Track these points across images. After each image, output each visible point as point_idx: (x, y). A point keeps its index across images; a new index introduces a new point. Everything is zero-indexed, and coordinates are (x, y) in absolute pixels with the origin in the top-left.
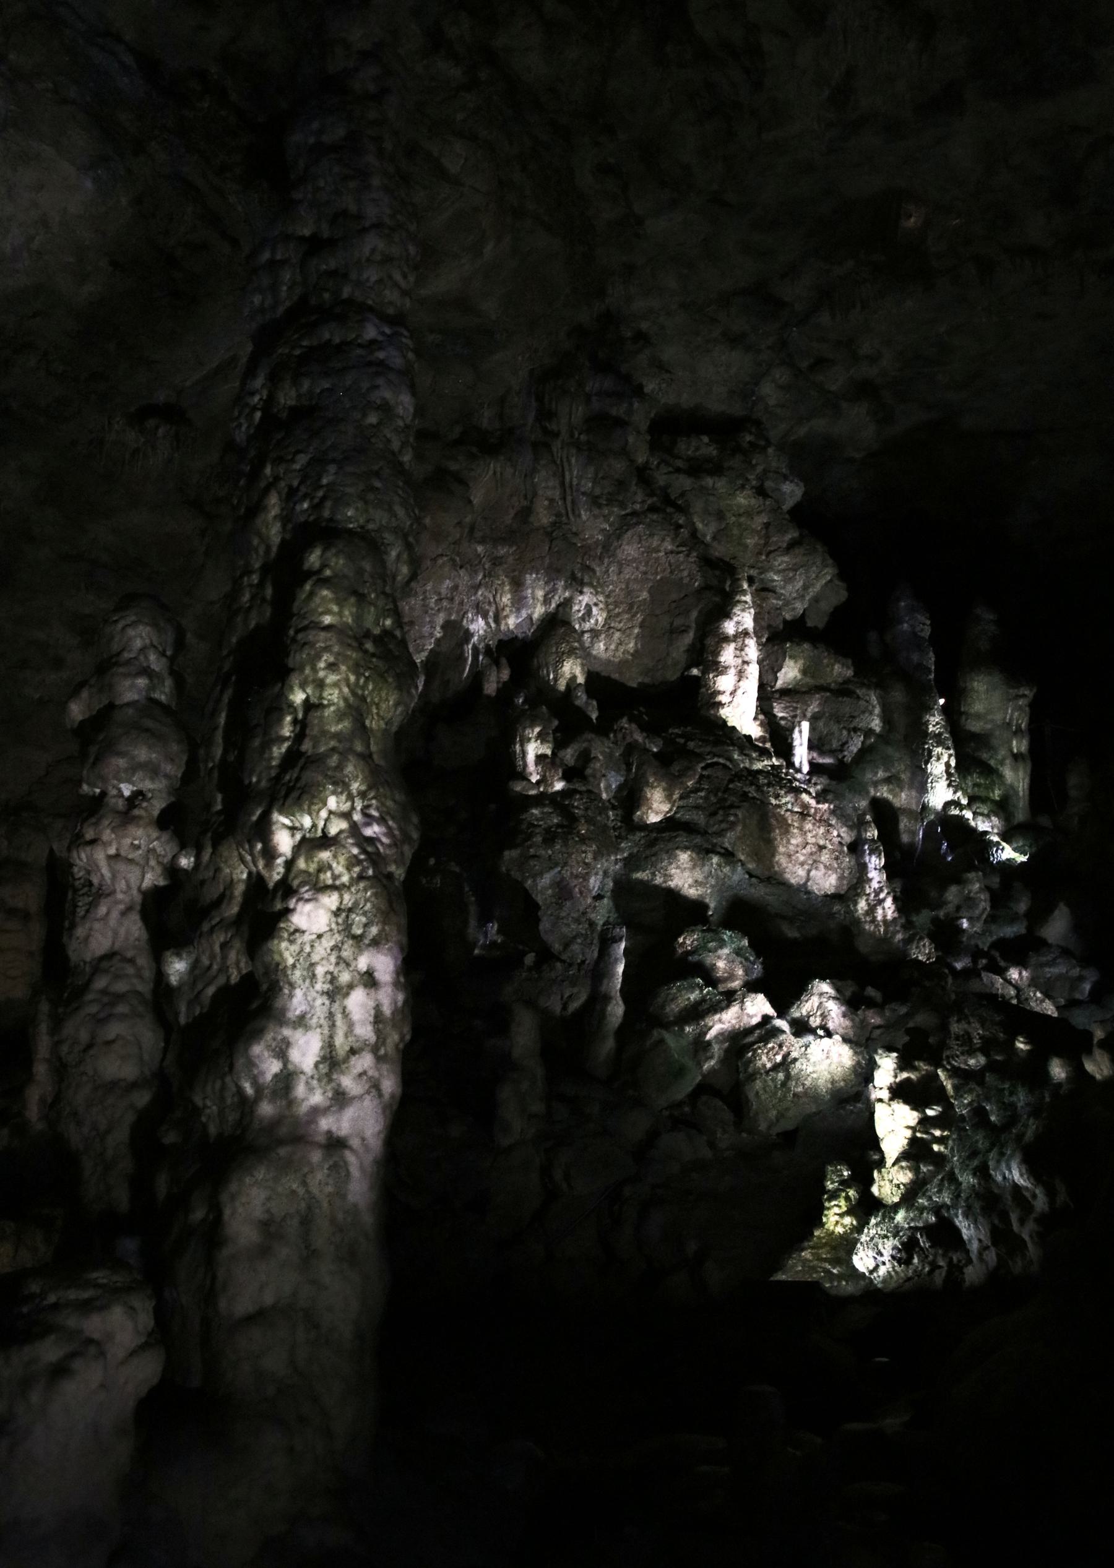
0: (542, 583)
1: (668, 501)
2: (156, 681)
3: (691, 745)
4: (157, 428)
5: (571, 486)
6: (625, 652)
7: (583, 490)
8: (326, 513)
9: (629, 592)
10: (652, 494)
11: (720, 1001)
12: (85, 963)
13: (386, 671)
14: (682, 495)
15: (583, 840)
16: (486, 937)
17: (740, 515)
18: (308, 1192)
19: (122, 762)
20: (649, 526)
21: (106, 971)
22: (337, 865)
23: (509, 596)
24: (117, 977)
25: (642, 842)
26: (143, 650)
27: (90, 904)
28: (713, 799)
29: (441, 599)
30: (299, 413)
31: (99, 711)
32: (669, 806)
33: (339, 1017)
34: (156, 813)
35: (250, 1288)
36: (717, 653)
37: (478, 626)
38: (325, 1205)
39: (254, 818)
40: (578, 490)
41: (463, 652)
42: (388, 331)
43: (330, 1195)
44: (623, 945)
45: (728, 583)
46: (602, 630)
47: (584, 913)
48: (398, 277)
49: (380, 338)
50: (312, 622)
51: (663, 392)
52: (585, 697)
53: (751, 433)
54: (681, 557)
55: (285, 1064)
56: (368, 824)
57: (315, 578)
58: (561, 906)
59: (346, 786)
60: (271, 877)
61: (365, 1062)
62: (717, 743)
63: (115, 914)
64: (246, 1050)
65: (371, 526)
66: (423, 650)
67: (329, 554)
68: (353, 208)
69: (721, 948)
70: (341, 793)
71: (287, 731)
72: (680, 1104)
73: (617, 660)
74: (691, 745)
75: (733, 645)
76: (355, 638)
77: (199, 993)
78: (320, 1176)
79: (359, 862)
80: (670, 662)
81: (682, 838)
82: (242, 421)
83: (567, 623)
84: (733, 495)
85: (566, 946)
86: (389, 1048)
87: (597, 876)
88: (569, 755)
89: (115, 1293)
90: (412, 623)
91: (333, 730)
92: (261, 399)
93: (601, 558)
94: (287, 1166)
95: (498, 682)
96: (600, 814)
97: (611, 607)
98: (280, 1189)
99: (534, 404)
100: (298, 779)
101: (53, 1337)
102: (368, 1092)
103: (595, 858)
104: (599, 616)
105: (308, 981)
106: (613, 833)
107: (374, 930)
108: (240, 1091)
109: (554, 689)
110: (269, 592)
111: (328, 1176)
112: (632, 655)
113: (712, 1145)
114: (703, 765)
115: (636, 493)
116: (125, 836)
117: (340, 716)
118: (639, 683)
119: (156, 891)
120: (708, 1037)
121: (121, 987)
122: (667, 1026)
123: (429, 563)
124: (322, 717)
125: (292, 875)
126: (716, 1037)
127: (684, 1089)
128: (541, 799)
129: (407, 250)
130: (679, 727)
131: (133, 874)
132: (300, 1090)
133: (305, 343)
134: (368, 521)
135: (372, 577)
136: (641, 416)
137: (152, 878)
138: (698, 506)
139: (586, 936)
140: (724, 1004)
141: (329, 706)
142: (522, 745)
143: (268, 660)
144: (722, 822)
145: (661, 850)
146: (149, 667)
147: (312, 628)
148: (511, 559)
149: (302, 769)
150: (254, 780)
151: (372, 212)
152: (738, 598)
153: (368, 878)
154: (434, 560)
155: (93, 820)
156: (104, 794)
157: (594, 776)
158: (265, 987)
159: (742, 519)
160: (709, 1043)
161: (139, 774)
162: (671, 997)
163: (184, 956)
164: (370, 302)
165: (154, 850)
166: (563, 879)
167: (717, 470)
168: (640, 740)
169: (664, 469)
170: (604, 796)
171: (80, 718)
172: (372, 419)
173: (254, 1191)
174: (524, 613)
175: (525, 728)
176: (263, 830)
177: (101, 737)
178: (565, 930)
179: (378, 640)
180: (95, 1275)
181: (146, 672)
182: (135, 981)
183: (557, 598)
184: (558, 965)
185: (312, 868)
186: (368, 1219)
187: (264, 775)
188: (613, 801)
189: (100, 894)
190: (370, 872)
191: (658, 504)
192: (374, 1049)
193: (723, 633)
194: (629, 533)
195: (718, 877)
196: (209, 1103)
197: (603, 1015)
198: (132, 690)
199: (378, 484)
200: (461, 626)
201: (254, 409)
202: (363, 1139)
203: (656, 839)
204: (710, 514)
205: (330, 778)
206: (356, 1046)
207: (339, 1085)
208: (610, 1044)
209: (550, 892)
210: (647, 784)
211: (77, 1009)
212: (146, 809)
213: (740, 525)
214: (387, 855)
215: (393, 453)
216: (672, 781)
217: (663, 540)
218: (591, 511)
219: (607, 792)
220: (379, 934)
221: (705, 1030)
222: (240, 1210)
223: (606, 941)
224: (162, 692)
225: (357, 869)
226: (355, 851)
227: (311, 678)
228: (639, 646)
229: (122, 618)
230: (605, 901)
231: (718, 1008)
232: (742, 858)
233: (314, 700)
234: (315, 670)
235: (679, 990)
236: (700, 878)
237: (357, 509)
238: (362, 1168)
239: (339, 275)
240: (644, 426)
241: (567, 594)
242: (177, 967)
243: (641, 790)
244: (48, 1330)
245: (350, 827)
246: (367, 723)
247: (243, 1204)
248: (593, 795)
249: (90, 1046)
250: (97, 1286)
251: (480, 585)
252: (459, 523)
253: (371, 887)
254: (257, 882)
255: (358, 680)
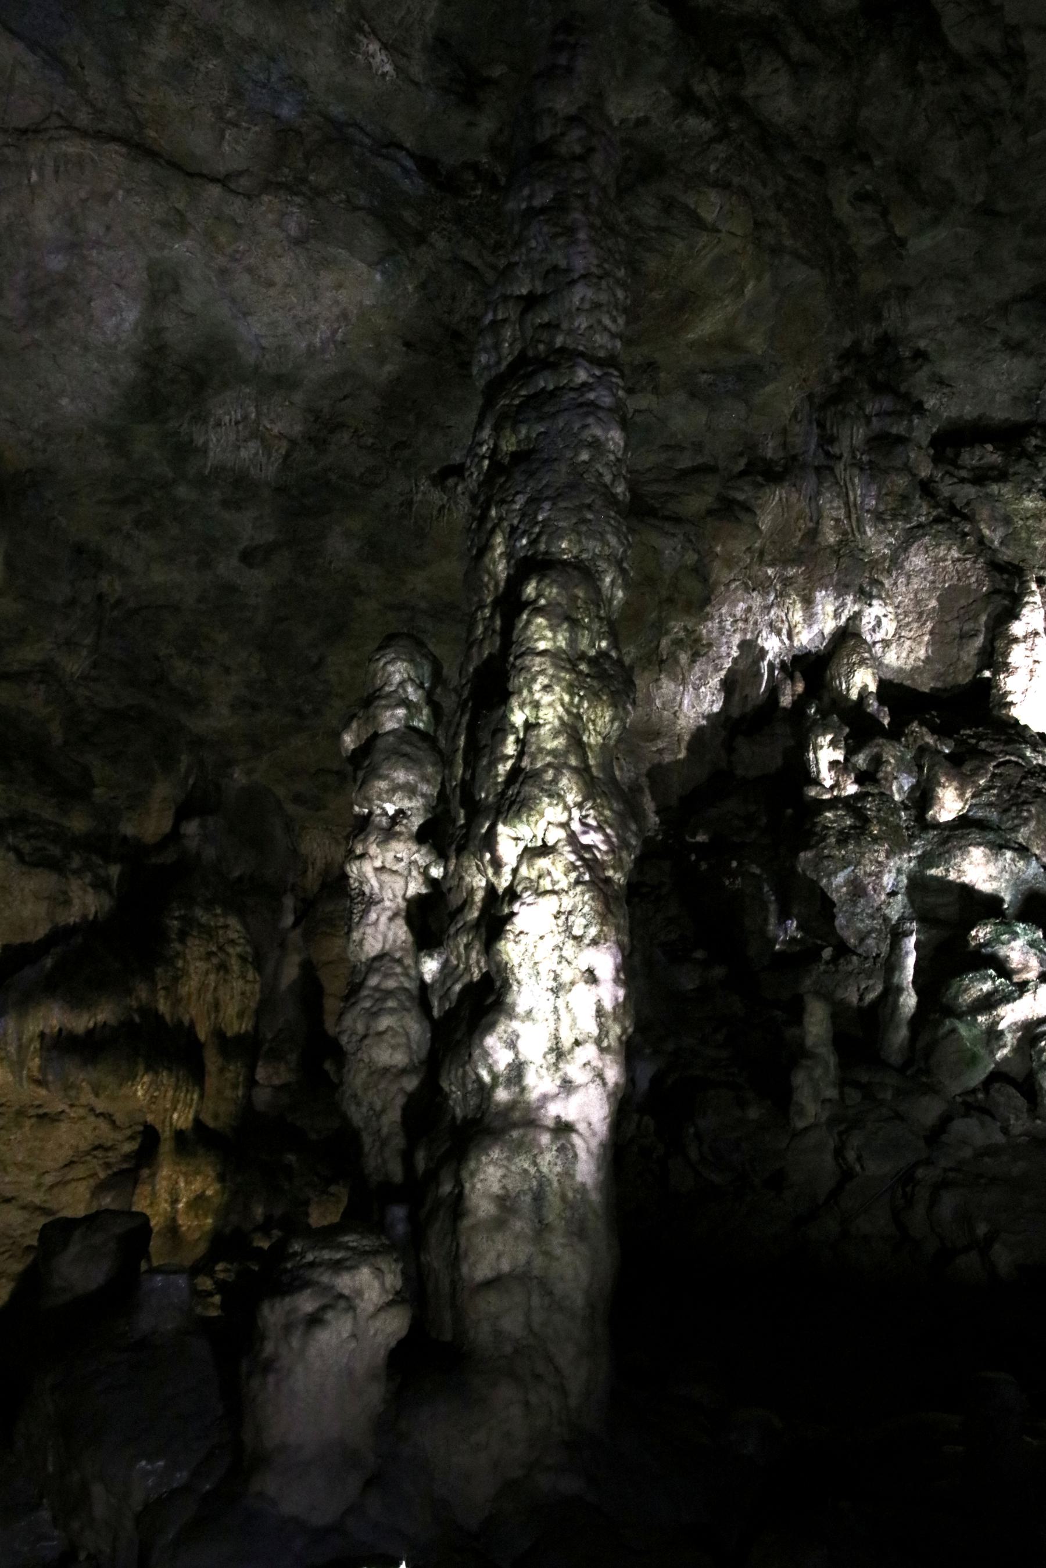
0: (831, 598)
1: (953, 510)
2: (414, 711)
3: (983, 745)
4: (456, 485)
5: (855, 505)
6: (917, 659)
7: (867, 507)
8: (542, 547)
9: (918, 602)
10: (937, 506)
11: (1012, 992)
12: (361, 963)
13: (601, 690)
14: (968, 504)
15: (876, 839)
16: (786, 933)
17: (1027, 518)
18: (538, 1171)
19: (383, 785)
20: (934, 537)
21: (378, 970)
22: (556, 869)
23: (801, 613)
24: (386, 976)
25: (936, 840)
26: (402, 684)
27: (363, 910)
28: (1006, 796)
29: (736, 621)
30: (519, 457)
31: (368, 740)
32: (961, 805)
33: (562, 1011)
34: (415, 829)
35: (491, 1256)
36: (1006, 654)
37: (772, 645)
38: (556, 1184)
39: (483, 831)
40: (862, 508)
41: (759, 669)
42: (598, 373)
43: (558, 1174)
44: (913, 939)
45: (1017, 585)
46: (894, 640)
47: (879, 909)
48: (607, 321)
49: (591, 380)
50: (528, 648)
51: (943, 407)
52: (876, 704)
53: (1036, 437)
54: (968, 564)
55: (517, 1055)
56: (585, 833)
57: (530, 608)
58: (855, 904)
59: (561, 797)
60: (499, 884)
61: (589, 1052)
62: (1010, 741)
63: (383, 919)
64: (482, 1040)
65: (584, 556)
66: (721, 669)
67: (543, 585)
68: (563, 264)
69: (1014, 939)
70: (557, 804)
71: (510, 749)
72: (974, 1091)
73: (908, 667)
74: (983, 745)
75: (1022, 645)
76: (569, 660)
77: (449, 988)
78: (548, 1156)
79: (575, 868)
80: (961, 665)
81: (975, 835)
82: (473, 470)
83: (857, 635)
84: (1020, 499)
85: (862, 940)
86: (611, 1040)
87: (891, 873)
88: (861, 760)
89: (364, 1255)
90: (710, 645)
91: (548, 747)
92: (488, 448)
93: (889, 572)
94: (519, 1147)
95: (793, 695)
96: (892, 815)
97: (901, 617)
98: (513, 1168)
99: (815, 430)
100: (519, 793)
101: (309, 1291)
102: (593, 1081)
103: (887, 857)
104: (889, 627)
105: (534, 978)
106: (905, 833)
107: (593, 931)
108: (479, 1079)
109: (846, 698)
110: (498, 623)
111: (557, 1157)
112: (923, 661)
113: (1005, 1130)
114: (994, 763)
115: (921, 506)
116: (387, 851)
117: (556, 734)
118: (932, 689)
119: (419, 899)
120: (1001, 1027)
121: (391, 984)
122: (960, 1016)
123: (723, 588)
124: (538, 735)
125: (516, 882)
126: (1009, 1027)
127: (977, 1077)
128: (835, 803)
129: (615, 296)
130: (970, 729)
131: (398, 884)
132: (530, 1079)
133: (523, 393)
134: (581, 551)
135: (586, 603)
136: (922, 430)
137: (416, 887)
138: (984, 513)
139: (880, 932)
140: (1016, 995)
141: (544, 724)
142: (815, 753)
143: (493, 687)
144: (1014, 818)
145: (954, 847)
146: (407, 698)
147: (528, 654)
148: (801, 579)
149: (522, 783)
150: (483, 795)
151: (580, 264)
152: (1026, 599)
153: (584, 883)
154: (727, 585)
155: (362, 837)
156: (371, 813)
157: (886, 779)
158: (498, 984)
159: (1030, 522)
160: (1002, 1032)
161: (399, 796)
162: (963, 987)
163: (436, 956)
164: (581, 348)
165: (415, 862)
166: (856, 877)
167: (1002, 476)
168: (931, 742)
169: (948, 480)
170: (897, 797)
171: (352, 747)
172: (585, 456)
173: (491, 1169)
174: (816, 629)
175: (817, 737)
176: (490, 841)
177: (366, 763)
178: (860, 925)
179: (592, 662)
180: (346, 1239)
181: (405, 703)
182: (402, 979)
183: (846, 612)
184: (855, 958)
185: (534, 875)
186: (595, 1197)
187: (492, 790)
188: (906, 802)
189: (371, 902)
190: (587, 877)
191: (944, 515)
192: (598, 1041)
193: (1012, 635)
194: (915, 545)
195: (1012, 872)
196: (454, 1089)
197: (896, 1006)
198: (392, 720)
199: (590, 516)
200: (757, 645)
201: (484, 457)
202: (590, 1124)
203: (949, 837)
204: (996, 520)
205: (546, 791)
206: (580, 1038)
207: (566, 1074)
208: (904, 1032)
209: (845, 889)
210: (939, 784)
211: (354, 1004)
212: (406, 826)
213: (1028, 528)
214: (604, 861)
215: (605, 486)
216: (963, 783)
217: (949, 549)
218: (876, 527)
219: (899, 794)
220: (598, 935)
221: (997, 1019)
222: (479, 1186)
223: (897, 935)
224: (420, 720)
225: (573, 875)
226: (572, 858)
227: (528, 701)
228: (930, 652)
229: (383, 656)
230: (899, 897)
231: (1008, 999)
232: (1037, 852)
233: (532, 720)
234: (530, 691)
235: (972, 981)
236: (994, 873)
237: (570, 541)
238: (588, 1151)
239: (552, 326)
240: (925, 443)
241: (856, 608)
242: (430, 967)
243: (934, 790)
244: (307, 1284)
245: (568, 835)
246: (585, 738)
247: (481, 1181)
248: (885, 797)
249: (365, 1036)
250: (348, 1248)
251: (772, 605)
252: (749, 549)
253: (589, 891)
254: (491, 889)
255: (572, 699)
